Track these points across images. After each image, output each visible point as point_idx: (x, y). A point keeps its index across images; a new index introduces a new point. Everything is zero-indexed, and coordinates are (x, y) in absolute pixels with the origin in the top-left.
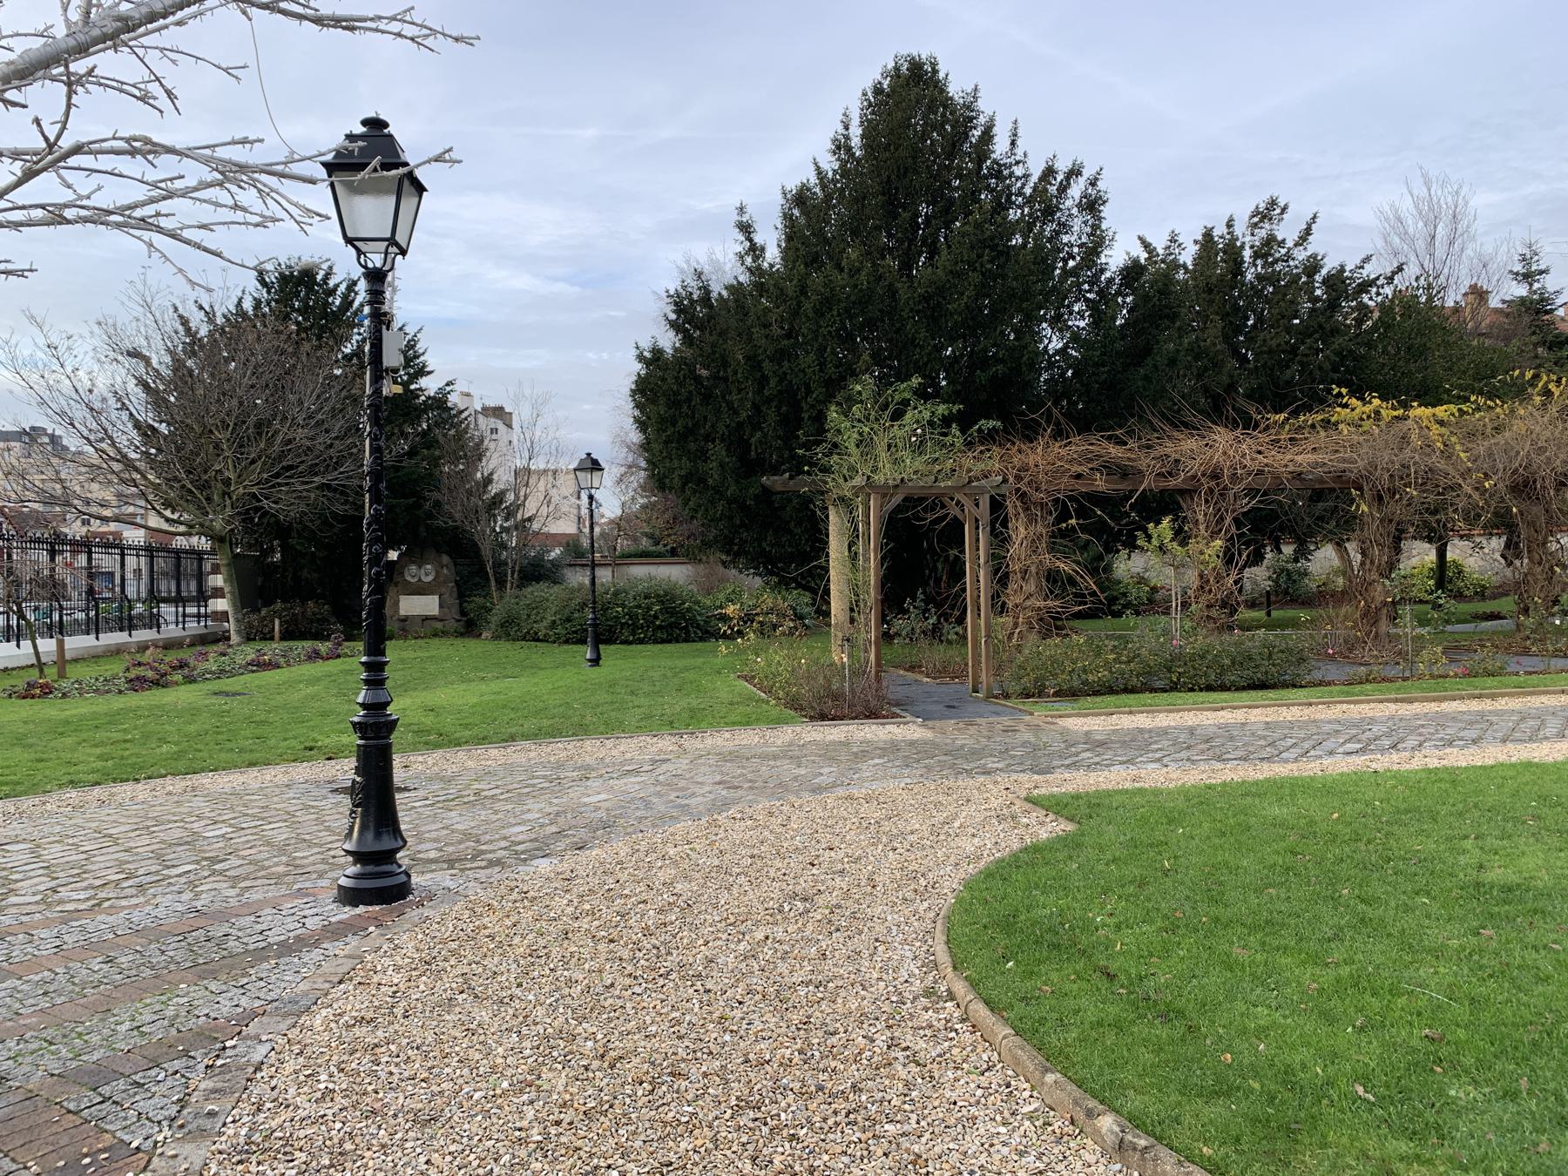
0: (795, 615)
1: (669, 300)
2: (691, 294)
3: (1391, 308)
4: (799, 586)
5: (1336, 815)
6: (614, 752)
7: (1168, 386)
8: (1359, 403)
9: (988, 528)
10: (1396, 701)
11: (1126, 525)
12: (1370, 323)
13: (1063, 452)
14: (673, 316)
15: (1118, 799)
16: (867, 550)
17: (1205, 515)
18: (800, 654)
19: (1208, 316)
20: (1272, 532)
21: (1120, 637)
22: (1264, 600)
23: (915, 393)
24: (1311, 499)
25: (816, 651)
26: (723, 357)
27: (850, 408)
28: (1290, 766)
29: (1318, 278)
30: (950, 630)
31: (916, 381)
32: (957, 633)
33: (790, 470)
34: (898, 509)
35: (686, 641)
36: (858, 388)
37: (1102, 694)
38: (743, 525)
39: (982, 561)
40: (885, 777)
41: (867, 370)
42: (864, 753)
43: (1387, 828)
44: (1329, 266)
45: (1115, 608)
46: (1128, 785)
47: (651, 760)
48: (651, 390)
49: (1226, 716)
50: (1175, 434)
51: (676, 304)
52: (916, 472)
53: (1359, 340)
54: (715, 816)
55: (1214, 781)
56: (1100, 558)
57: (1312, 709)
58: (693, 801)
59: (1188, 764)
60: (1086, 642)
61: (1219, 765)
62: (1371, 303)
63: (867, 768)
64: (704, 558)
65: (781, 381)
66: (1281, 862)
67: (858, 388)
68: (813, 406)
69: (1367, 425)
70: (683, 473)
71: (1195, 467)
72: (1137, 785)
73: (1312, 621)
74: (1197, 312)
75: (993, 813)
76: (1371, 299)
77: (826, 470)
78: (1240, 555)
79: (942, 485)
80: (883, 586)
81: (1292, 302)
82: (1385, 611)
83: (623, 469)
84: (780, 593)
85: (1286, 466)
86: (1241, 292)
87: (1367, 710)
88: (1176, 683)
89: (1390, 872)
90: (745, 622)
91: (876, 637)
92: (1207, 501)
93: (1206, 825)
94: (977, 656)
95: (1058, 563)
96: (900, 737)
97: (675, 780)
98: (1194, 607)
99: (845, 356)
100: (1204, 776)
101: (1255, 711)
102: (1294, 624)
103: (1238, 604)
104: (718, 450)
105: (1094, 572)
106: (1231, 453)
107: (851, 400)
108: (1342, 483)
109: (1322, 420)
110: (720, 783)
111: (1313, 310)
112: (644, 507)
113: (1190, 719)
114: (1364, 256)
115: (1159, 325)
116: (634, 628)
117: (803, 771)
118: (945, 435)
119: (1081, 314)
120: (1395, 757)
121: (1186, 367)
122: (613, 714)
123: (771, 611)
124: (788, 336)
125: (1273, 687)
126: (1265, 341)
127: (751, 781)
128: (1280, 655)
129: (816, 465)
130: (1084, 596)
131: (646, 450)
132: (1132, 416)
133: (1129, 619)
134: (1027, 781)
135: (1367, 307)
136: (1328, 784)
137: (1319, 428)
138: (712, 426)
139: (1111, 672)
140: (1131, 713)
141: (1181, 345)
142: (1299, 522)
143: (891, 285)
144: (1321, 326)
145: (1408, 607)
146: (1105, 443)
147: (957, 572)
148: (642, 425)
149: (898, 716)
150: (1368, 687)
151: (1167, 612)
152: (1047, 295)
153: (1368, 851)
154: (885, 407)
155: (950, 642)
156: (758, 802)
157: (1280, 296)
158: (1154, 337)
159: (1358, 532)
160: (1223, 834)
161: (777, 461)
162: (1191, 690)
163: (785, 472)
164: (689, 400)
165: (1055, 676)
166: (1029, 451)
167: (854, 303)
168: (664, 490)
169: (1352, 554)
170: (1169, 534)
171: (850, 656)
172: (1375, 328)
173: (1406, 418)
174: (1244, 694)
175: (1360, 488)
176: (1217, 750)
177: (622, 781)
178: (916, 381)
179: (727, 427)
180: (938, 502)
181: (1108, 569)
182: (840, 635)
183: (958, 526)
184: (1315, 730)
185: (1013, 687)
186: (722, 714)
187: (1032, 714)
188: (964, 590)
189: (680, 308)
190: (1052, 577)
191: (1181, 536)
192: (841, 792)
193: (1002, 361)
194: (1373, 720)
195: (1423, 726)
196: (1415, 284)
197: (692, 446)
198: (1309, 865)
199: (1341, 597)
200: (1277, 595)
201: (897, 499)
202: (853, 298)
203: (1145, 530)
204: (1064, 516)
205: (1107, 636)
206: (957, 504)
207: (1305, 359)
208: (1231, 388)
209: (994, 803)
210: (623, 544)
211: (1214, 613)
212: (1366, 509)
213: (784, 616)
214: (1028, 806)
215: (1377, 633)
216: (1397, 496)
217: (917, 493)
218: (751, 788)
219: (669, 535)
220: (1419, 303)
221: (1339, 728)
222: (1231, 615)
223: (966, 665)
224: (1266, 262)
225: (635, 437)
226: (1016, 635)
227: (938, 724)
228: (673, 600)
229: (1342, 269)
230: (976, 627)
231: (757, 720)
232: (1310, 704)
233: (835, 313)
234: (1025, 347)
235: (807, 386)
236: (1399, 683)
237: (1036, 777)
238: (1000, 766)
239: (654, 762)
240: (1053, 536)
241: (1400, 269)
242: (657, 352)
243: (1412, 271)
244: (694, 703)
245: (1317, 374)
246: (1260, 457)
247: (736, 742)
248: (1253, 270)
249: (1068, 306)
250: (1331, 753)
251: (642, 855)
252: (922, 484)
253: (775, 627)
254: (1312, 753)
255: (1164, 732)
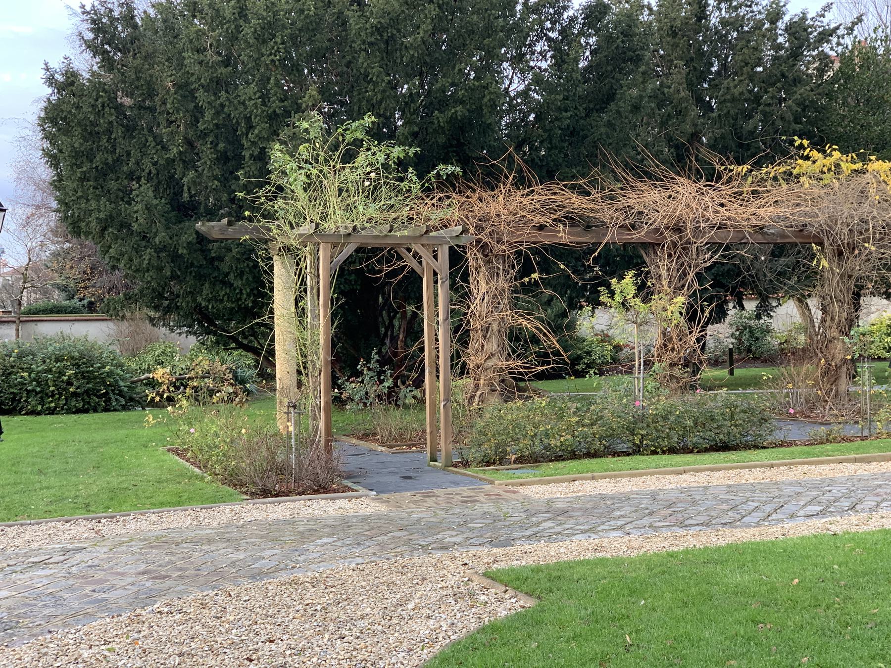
0: (236, 378)
1: (85, 17)
2: (111, 11)
3: (851, 59)
4: (240, 346)
5: (797, 580)
6: (18, 542)
7: (632, 134)
8: (820, 155)
9: (447, 283)
10: (856, 461)
11: (590, 280)
12: (831, 73)
13: (525, 201)
14: (90, 36)
15: (581, 570)
16: (315, 306)
17: (668, 270)
18: (240, 423)
19: (672, 61)
20: (734, 289)
21: (583, 398)
22: (727, 358)
23: (367, 133)
24: (773, 254)
25: (258, 419)
26: (149, 83)
27: (296, 148)
28: (752, 531)
29: (781, 25)
30: (407, 394)
31: (369, 120)
32: (414, 397)
33: (229, 214)
34: (349, 261)
35: (106, 410)
36: (305, 125)
37: (564, 460)
38: (173, 277)
39: (441, 318)
40: (333, 558)
41: (314, 106)
42: (311, 532)
43: (845, 592)
44: (792, 12)
45: (579, 367)
46: (589, 556)
47: (62, 549)
48: (64, 119)
49: (688, 480)
50: (639, 184)
51: (94, 22)
52: (369, 220)
53: (820, 90)
54: (138, 611)
55: (675, 549)
56: (564, 315)
57: (774, 471)
58: (111, 596)
59: (651, 531)
60: (548, 404)
61: (681, 532)
62: (833, 54)
63: (314, 549)
64: (128, 314)
65: (217, 113)
66: (742, 632)
67: (305, 125)
68: (254, 143)
69: (828, 178)
70: (102, 215)
71: (658, 219)
72: (599, 555)
73: (774, 380)
74: (661, 56)
75: (450, 591)
76: (832, 49)
77: (269, 216)
78: (703, 311)
79: (398, 234)
80: (334, 345)
81: (755, 49)
82: (844, 369)
83: (30, 211)
84: (217, 353)
85: (748, 219)
86: (705, 36)
87: (825, 471)
88: (639, 447)
89: (848, 637)
90: (177, 388)
91: (326, 403)
92: (670, 256)
93: (668, 596)
94: (435, 421)
95: (521, 320)
96: (351, 513)
97: (91, 572)
98: (657, 366)
99: (290, 89)
100: (666, 544)
101: (717, 474)
102: (756, 382)
103: (701, 362)
104: (144, 192)
105: (556, 329)
106: (694, 205)
107: (297, 139)
108: (804, 237)
109: (785, 172)
110: (143, 573)
111: (775, 58)
112: (56, 255)
113: (652, 483)
114: (824, 4)
115: (622, 69)
116: (43, 396)
117: (241, 556)
118: (401, 180)
119: (543, 54)
120: (854, 518)
121: (648, 115)
122: (17, 497)
123: (206, 375)
124: (227, 63)
125: (736, 448)
126: (728, 88)
127: (181, 569)
128: (742, 415)
129: (258, 210)
130: (546, 355)
131: (57, 188)
132: (596, 165)
133: (593, 379)
134: (486, 553)
135: (827, 56)
136: (789, 549)
137: (781, 181)
138: (137, 163)
139: (574, 436)
140: (593, 478)
141: (644, 90)
142: (762, 277)
143: (341, 13)
144: (783, 75)
145: (866, 365)
146: (568, 193)
147: (414, 331)
148: (53, 160)
149: (350, 489)
150: (829, 447)
151: (630, 371)
152: (509, 31)
153: (827, 616)
154: (335, 148)
155: (406, 407)
156: (189, 593)
157: (744, 42)
158: (618, 81)
159: (819, 288)
160: (686, 604)
161: (215, 205)
162: (654, 453)
163: (223, 216)
164: (109, 132)
165: (516, 440)
166: (490, 199)
167: (300, 30)
168: (79, 235)
169: (813, 310)
170: (631, 290)
171: (297, 424)
172: (834, 80)
173: (863, 172)
174: (706, 457)
175: (821, 244)
176: (679, 515)
177: (27, 575)
178: (369, 120)
179: (155, 164)
180: (393, 254)
181: (571, 326)
182: (286, 401)
183: (414, 280)
184: (777, 493)
185: (473, 454)
186: (147, 494)
187: (492, 483)
188: (422, 350)
189: (98, 27)
190: (515, 335)
191: (644, 291)
192: (284, 577)
193: (462, 102)
194: (832, 482)
195: (880, 486)
196: (874, 36)
197: (113, 185)
198: (770, 634)
199: (801, 355)
200: (740, 353)
201: (349, 250)
202: (299, 25)
203: (608, 286)
204: (526, 270)
205: (570, 398)
206: (414, 256)
207: (767, 109)
208: (695, 137)
209: (451, 581)
210: (29, 298)
211: (677, 372)
212: (827, 265)
213: (223, 380)
214: (486, 582)
215: (837, 391)
216: (857, 252)
217: (372, 243)
218: (181, 577)
219: (86, 288)
220: (877, 55)
221: (798, 489)
222: (694, 373)
223: (424, 431)
224: (730, 6)
225: (46, 173)
226: (477, 399)
227: (392, 496)
228: (91, 362)
229: (804, 18)
230: (434, 390)
231: (190, 499)
232: (772, 466)
233: (279, 40)
234: (486, 87)
235: (248, 119)
236: (859, 442)
237: (495, 550)
238: (458, 539)
239: (65, 551)
240: (515, 291)
241: (860, 20)
242: (71, 77)
243: (871, 21)
244: (115, 482)
245: (780, 124)
246: (722, 209)
247: (165, 526)
248: (717, 14)
249: (530, 46)
250: (792, 516)
251: (50, 659)
252: (376, 233)
253: (211, 392)
254: (774, 516)
255: (626, 498)
